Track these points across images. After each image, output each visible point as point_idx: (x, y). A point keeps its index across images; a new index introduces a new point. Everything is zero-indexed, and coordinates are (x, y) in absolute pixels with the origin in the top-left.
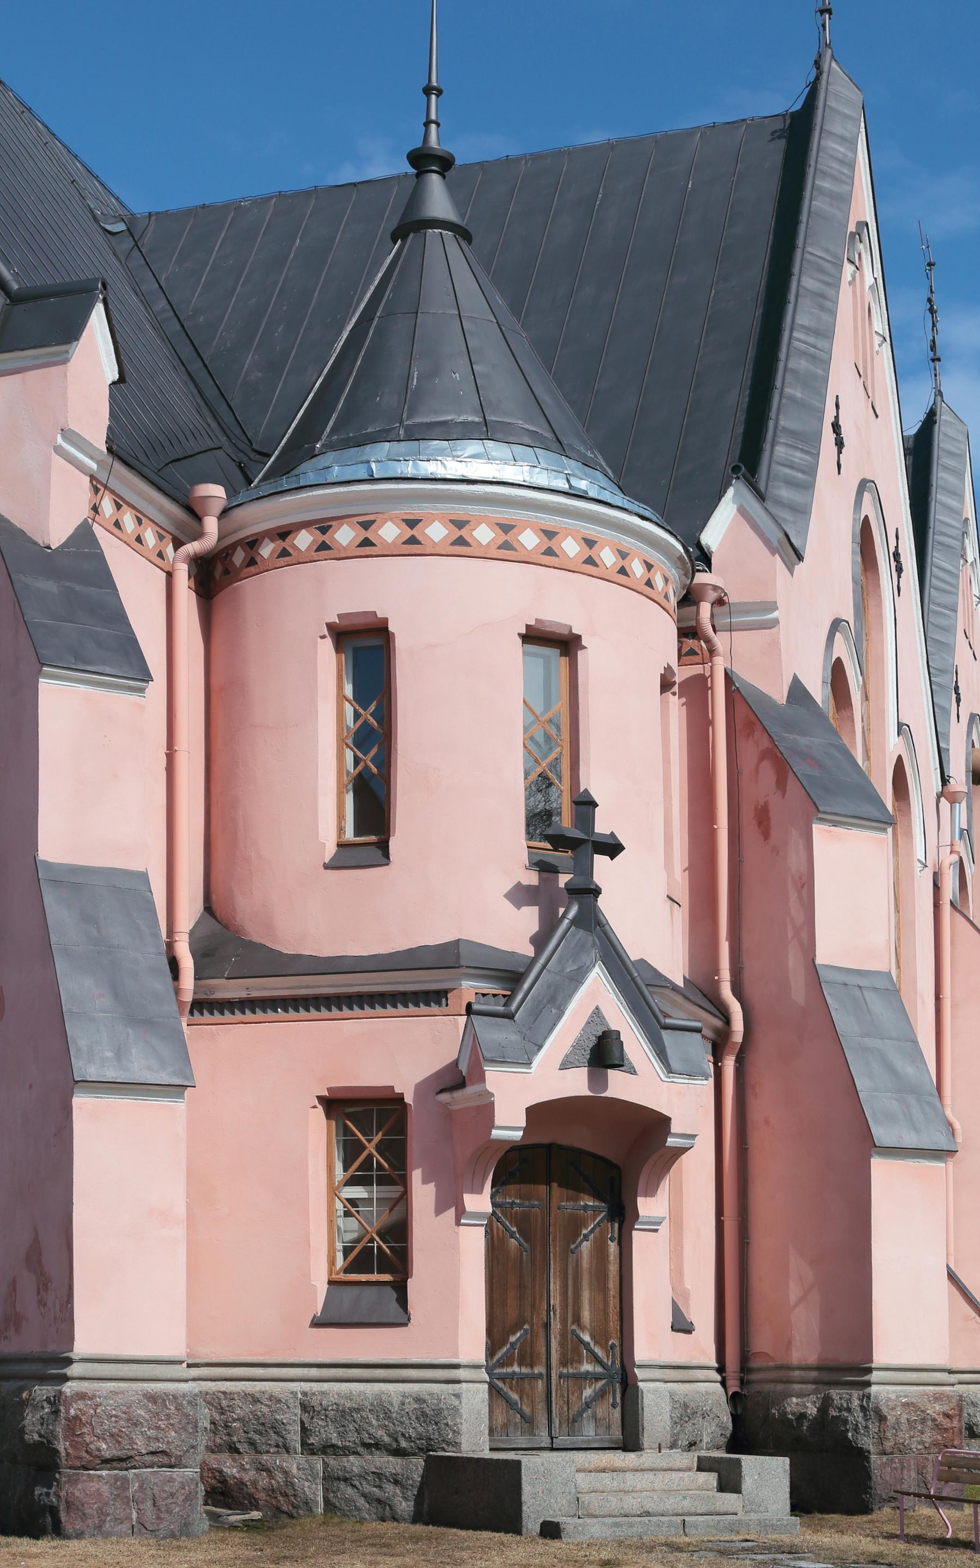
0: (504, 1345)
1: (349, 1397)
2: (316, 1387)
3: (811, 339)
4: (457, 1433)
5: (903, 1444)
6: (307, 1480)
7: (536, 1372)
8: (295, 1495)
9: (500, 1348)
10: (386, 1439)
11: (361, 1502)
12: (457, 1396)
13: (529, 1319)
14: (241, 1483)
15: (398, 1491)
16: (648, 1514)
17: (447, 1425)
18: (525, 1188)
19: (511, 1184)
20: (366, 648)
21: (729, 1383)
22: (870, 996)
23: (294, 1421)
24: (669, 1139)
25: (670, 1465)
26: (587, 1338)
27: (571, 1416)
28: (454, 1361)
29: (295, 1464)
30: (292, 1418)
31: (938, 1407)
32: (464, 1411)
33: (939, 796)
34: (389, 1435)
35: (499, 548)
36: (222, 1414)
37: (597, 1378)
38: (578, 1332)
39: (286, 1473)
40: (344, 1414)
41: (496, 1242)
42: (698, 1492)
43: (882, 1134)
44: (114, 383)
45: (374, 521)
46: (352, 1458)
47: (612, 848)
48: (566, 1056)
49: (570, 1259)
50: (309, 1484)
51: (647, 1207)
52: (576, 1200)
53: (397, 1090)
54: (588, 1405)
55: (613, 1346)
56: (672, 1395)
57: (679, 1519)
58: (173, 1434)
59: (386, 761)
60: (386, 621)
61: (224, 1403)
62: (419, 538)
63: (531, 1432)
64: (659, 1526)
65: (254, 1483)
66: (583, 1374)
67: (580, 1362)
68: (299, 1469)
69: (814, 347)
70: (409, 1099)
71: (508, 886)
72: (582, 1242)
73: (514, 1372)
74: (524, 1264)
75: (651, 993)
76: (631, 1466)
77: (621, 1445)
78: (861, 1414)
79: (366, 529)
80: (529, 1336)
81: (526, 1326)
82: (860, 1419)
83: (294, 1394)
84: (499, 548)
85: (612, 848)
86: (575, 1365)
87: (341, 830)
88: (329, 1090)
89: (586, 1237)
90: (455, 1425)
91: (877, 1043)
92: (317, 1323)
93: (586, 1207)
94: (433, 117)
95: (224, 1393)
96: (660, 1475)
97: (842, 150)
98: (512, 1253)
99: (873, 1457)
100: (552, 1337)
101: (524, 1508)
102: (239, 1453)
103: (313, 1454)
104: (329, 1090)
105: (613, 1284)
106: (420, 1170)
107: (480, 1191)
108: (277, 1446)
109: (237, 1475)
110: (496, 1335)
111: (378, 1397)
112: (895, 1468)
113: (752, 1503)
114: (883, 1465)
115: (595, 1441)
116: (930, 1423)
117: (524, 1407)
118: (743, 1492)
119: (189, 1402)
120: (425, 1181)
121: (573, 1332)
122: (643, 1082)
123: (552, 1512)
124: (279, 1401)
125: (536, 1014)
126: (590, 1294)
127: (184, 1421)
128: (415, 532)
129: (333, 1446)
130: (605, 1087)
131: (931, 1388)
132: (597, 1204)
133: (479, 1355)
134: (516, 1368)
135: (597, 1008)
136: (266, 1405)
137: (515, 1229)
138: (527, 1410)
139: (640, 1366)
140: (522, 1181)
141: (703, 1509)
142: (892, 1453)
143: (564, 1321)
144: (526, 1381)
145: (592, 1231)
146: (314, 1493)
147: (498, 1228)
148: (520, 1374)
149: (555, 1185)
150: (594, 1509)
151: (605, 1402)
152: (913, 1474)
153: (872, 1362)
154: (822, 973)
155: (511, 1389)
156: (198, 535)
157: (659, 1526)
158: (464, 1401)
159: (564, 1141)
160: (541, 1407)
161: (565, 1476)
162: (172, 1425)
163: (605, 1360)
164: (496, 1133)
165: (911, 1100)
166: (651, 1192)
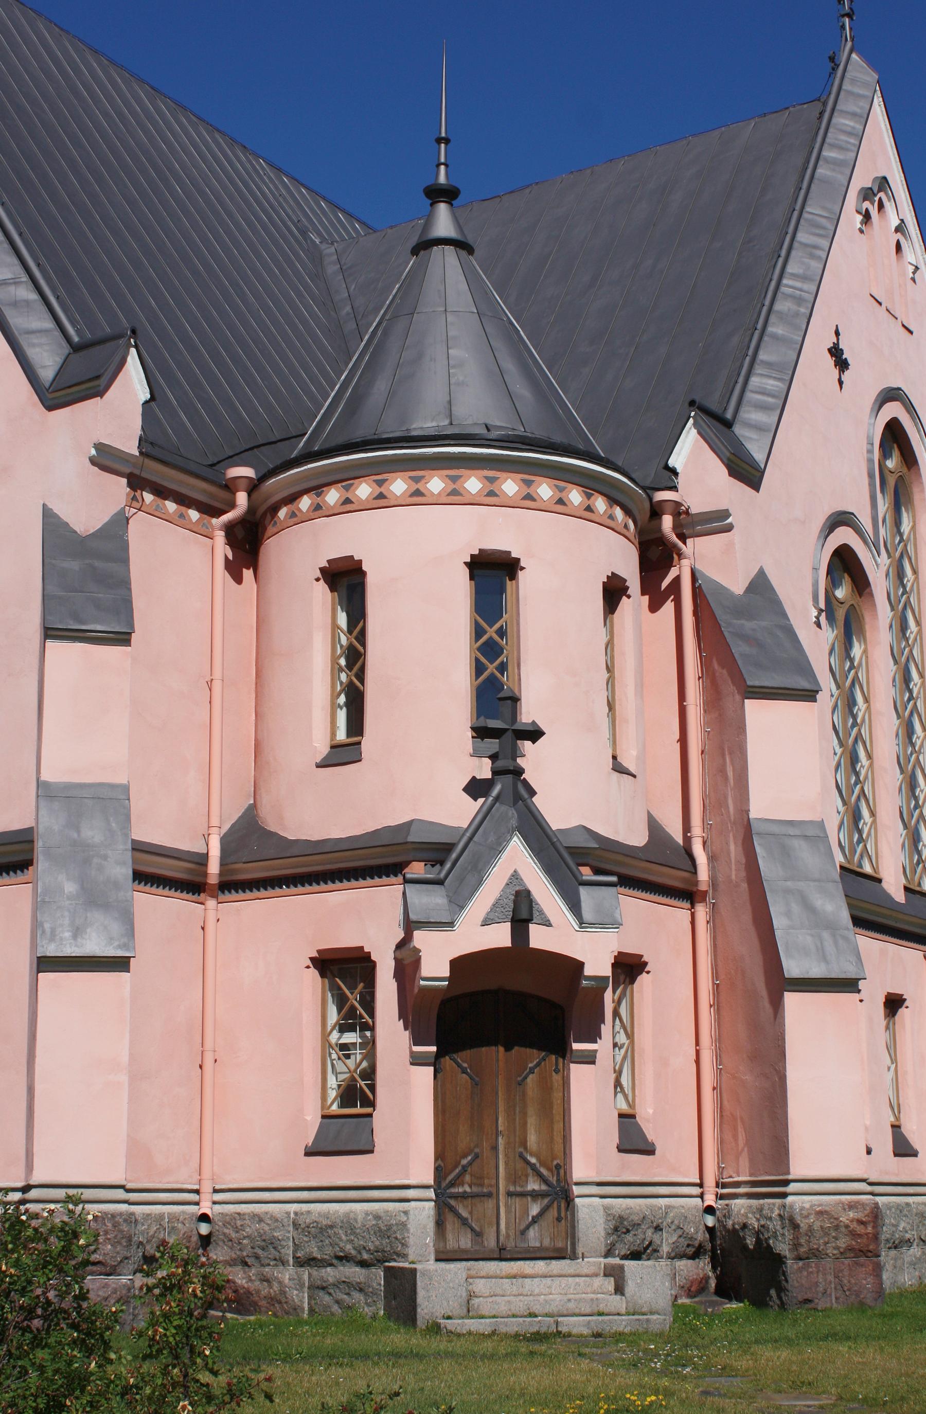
0: (456, 1167)
1: (327, 1216)
2: (305, 1207)
3: (798, 284)
5: (817, 1249)
8: (286, 1302)
10: (353, 1252)
11: (335, 1308)
14: (248, 1292)
15: (362, 1298)
17: (396, 1238)
21: (706, 1197)
22: (796, 843)
23: (288, 1238)
25: (577, 1272)
29: (287, 1274)
30: (287, 1235)
31: (851, 1214)
32: (412, 1227)
34: (354, 1248)
35: (448, 495)
36: (237, 1232)
38: (525, 1154)
39: (280, 1283)
40: (322, 1230)
42: (592, 1296)
43: (793, 968)
44: (146, 402)
45: (424, 477)
46: (329, 1269)
47: (535, 734)
48: (488, 914)
53: (366, 950)
57: (552, 1320)
58: (109, 1247)
59: (361, 675)
60: (360, 562)
61: (239, 1223)
62: (385, 493)
65: (258, 1292)
68: (290, 1279)
69: (801, 290)
76: (540, 1273)
78: (779, 1223)
79: (380, 486)
82: (778, 1227)
83: (288, 1213)
84: (448, 495)
85: (535, 734)
87: (333, 734)
88: (319, 951)
89: (532, 1071)
90: (403, 1238)
91: (801, 885)
94: (443, 160)
95: (239, 1214)
96: (557, 1281)
97: (852, 124)
99: (789, 1262)
101: (419, 1310)
102: (249, 1266)
103: (302, 1266)
104: (319, 951)
108: (275, 1259)
109: (246, 1286)
111: (347, 1215)
112: (811, 1272)
114: (800, 1270)
116: (843, 1229)
118: (627, 1295)
119: (125, 1220)
124: (277, 1220)
125: (461, 880)
127: (120, 1236)
128: (382, 490)
129: (314, 1259)
131: (848, 1197)
136: (268, 1224)
139: (577, 1184)
142: (808, 1258)
152: (831, 1278)
153: (788, 1173)
154: (755, 827)
158: (411, 1217)
162: (109, 1239)
163: (551, 1179)
164: (422, 983)
165: (826, 935)
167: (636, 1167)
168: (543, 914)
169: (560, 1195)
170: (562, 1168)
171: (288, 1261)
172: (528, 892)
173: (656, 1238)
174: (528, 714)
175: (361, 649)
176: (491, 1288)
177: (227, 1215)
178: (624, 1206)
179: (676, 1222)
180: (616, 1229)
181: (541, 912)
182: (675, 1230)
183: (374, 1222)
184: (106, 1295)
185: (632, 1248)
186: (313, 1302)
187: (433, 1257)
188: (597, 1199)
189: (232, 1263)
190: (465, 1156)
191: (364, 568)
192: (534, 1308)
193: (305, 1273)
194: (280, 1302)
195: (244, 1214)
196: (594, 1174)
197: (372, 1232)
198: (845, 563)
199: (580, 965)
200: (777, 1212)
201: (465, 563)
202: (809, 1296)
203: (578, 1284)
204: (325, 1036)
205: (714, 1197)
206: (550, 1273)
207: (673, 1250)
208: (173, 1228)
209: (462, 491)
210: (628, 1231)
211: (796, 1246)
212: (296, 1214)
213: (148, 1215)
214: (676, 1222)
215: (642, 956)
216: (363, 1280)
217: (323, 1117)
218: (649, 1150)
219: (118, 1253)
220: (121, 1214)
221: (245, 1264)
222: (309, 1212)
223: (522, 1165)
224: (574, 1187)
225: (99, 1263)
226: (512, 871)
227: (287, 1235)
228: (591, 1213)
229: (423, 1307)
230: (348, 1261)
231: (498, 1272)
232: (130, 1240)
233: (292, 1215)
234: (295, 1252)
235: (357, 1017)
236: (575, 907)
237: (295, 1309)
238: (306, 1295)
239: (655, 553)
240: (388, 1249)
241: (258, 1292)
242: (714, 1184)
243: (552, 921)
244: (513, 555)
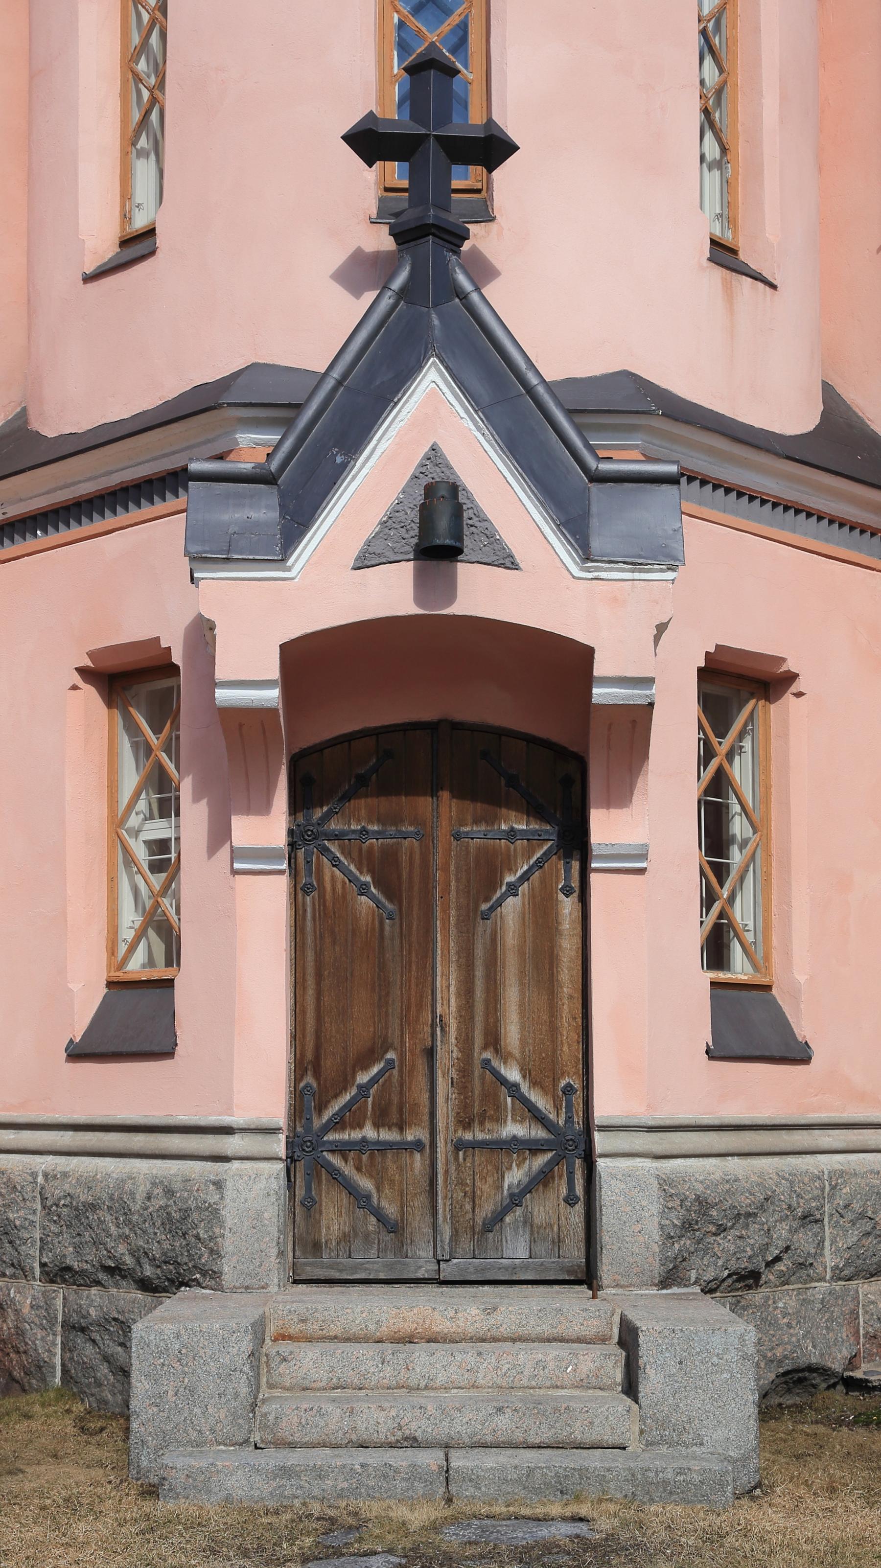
1: (88, 1183)
4: (216, 1253)
6: (43, 1328)
7: (410, 1138)
8: (25, 1352)
9: (336, 1096)
10: (129, 1260)
11: (104, 1369)
12: (218, 1185)
13: (397, 1042)
16: (413, 1442)
17: (197, 1237)
18: (384, 804)
19: (359, 798)
24: (595, 691)
26: (513, 1074)
27: (479, 1221)
28: (226, 1120)
32: (229, 1214)
34: (132, 1253)
37: (534, 1148)
38: (495, 1063)
40: (75, 1213)
41: (329, 904)
46: (94, 1291)
47: (368, 142)
48: (368, 543)
49: (480, 930)
50: (44, 1333)
51: (605, 828)
52: (491, 820)
53: (164, 644)
54: (515, 1200)
55: (569, 1090)
56: (665, 1183)
57: (431, 1459)
63: (400, 1250)
64: (385, 1476)
66: (505, 1142)
67: (499, 1119)
68: (32, 1307)
70: (177, 658)
71: (338, 257)
73: (364, 1140)
74: (387, 942)
76: (471, 1330)
77: (580, 1276)
80: (395, 1072)
81: (391, 1055)
83: (34, 1175)
85: (368, 142)
86: (488, 1125)
88: (91, 655)
89: (513, 890)
90: (211, 1238)
92: (77, 1054)
93: (512, 835)
98: (363, 922)
100: (439, 1073)
103: (52, 1281)
104: (91, 655)
105: (567, 976)
106: (191, 777)
107: (264, 808)
110: (315, 1069)
113: (663, 1424)
115: (526, 1267)
117: (384, 1204)
118: (642, 1401)
120: (196, 799)
121: (486, 1063)
123: (194, 1435)
126: (522, 992)
129: (69, 1269)
130: (451, 596)
132: (534, 826)
133: (274, 1107)
137: (368, 879)
138: (391, 1209)
139: (603, 1128)
140: (386, 789)
141: (545, 1435)
143: (466, 1042)
144: (389, 1154)
145: (525, 877)
146: (49, 1351)
147: (333, 877)
148: (378, 1142)
149: (445, 795)
150: (289, 1428)
151: (551, 1195)
155: (359, 1169)
157: (385, 1476)
158: (229, 1193)
160: (420, 1202)
161: (225, 1360)
164: (222, 695)
166: (621, 795)
167: (759, 1091)
168: (499, 541)
169: (574, 1147)
172: (454, 489)
173: (804, 1240)
176: (332, 1369)
178: (717, 1176)
179: (856, 1206)
180: (688, 1226)
182: (853, 1223)
185: (733, 1265)
188: (647, 1163)
190: (364, 1063)
192: (413, 1426)
193: (59, 1295)
197: (158, 1223)
199: (584, 655)
203: (540, 1364)
206: (495, 1333)
207: (848, 1264)
210: (722, 1229)
214: (856, 1206)
215: (783, 660)
217: (110, 984)
218: (797, 1055)
222: (65, 1175)
226: (427, 448)
227: (29, 1217)
228: (631, 1190)
229: (143, 1417)
230: (124, 1277)
231: (372, 1327)
233: (40, 1179)
237: (40, 1367)
238: (59, 1340)
240: (185, 1259)
243: (518, 559)
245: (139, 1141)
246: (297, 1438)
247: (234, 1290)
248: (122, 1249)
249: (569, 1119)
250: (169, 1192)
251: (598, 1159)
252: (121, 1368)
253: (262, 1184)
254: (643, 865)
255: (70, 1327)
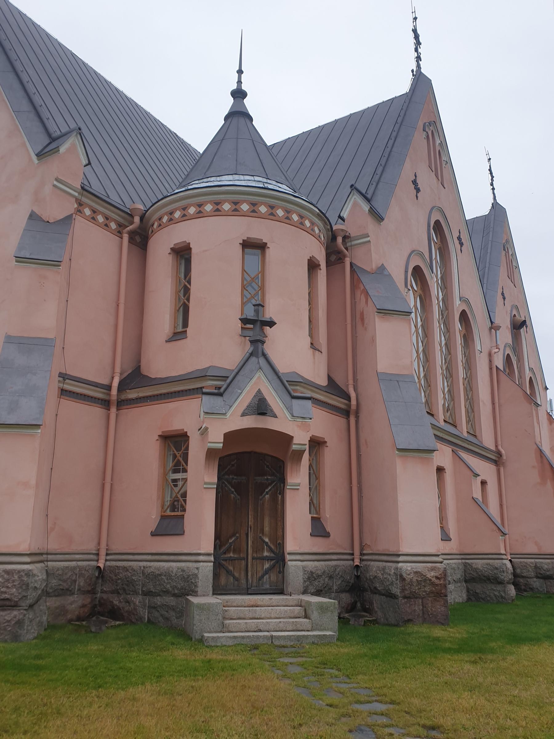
2: (148, 564)
4: (196, 586)
5: (415, 592)
6: (142, 608)
10: (170, 589)
11: (161, 619)
14: (119, 609)
17: (192, 582)
20: (183, 254)
21: (355, 560)
23: (140, 580)
26: (267, 540)
28: (199, 552)
33: (491, 328)
40: (155, 577)
47: (271, 324)
48: (244, 410)
58: (15, 590)
65: (123, 608)
72: (265, 495)
75: (289, 385)
81: (238, 535)
83: (140, 567)
85: (271, 324)
88: (162, 432)
89: (267, 493)
92: (153, 534)
95: (117, 566)
103: (146, 595)
104: (162, 432)
116: (428, 582)
119: (26, 574)
122: (282, 421)
133: (210, 549)
134: (232, 555)
135: (259, 389)
138: (237, 575)
156: (132, 223)
158: (200, 571)
159: (258, 450)
160: (243, 574)
162: (15, 585)
169: (279, 559)
170: (281, 545)
171: (139, 592)
174: (270, 313)
175: (188, 286)
177: (112, 567)
180: (309, 578)
181: (272, 410)
183: (181, 573)
184: (9, 619)
186: (150, 615)
187: (211, 593)
188: (300, 563)
189: (112, 592)
190: (231, 537)
191: (191, 246)
194: (134, 614)
195: (120, 567)
196: (298, 549)
198: (417, 271)
200: (393, 571)
201: (240, 244)
202: (410, 617)
204: (165, 474)
205: (359, 560)
208: (81, 573)
209: (239, 210)
210: (315, 579)
211: (403, 590)
212: (144, 567)
213: (67, 567)
214: (340, 574)
216: (174, 604)
219: (19, 593)
220: (23, 570)
221: (118, 593)
222: (150, 567)
223: (259, 545)
224: (288, 556)
225: (8, 599)
228: (295, 569)
232: (28, 585)
234: (142, 588)
235: (180, 465)
236: (290, 409)
239: (333, 258)
241: (123, 608)
242: (359, 554)
244: (264, 241)
245: (172, 558)
246: (233, 630)
247: (201, 596)
248: (168, 586)
249: (279, 551)
250: (183, 571)
251: (289, 563)
252: (401, 576)
253: (209, 568)
254: (298, 487)
255: (150, 607)
